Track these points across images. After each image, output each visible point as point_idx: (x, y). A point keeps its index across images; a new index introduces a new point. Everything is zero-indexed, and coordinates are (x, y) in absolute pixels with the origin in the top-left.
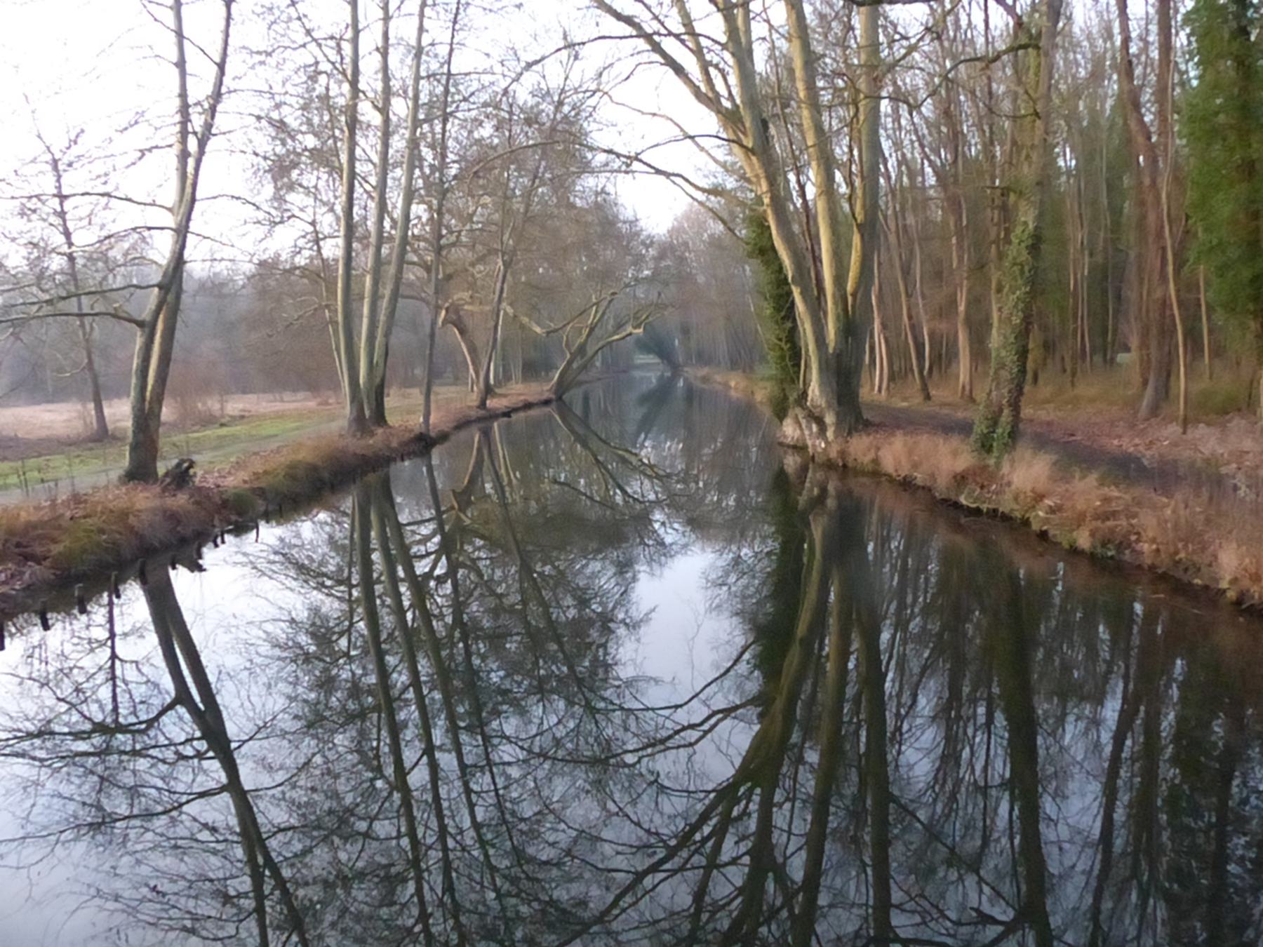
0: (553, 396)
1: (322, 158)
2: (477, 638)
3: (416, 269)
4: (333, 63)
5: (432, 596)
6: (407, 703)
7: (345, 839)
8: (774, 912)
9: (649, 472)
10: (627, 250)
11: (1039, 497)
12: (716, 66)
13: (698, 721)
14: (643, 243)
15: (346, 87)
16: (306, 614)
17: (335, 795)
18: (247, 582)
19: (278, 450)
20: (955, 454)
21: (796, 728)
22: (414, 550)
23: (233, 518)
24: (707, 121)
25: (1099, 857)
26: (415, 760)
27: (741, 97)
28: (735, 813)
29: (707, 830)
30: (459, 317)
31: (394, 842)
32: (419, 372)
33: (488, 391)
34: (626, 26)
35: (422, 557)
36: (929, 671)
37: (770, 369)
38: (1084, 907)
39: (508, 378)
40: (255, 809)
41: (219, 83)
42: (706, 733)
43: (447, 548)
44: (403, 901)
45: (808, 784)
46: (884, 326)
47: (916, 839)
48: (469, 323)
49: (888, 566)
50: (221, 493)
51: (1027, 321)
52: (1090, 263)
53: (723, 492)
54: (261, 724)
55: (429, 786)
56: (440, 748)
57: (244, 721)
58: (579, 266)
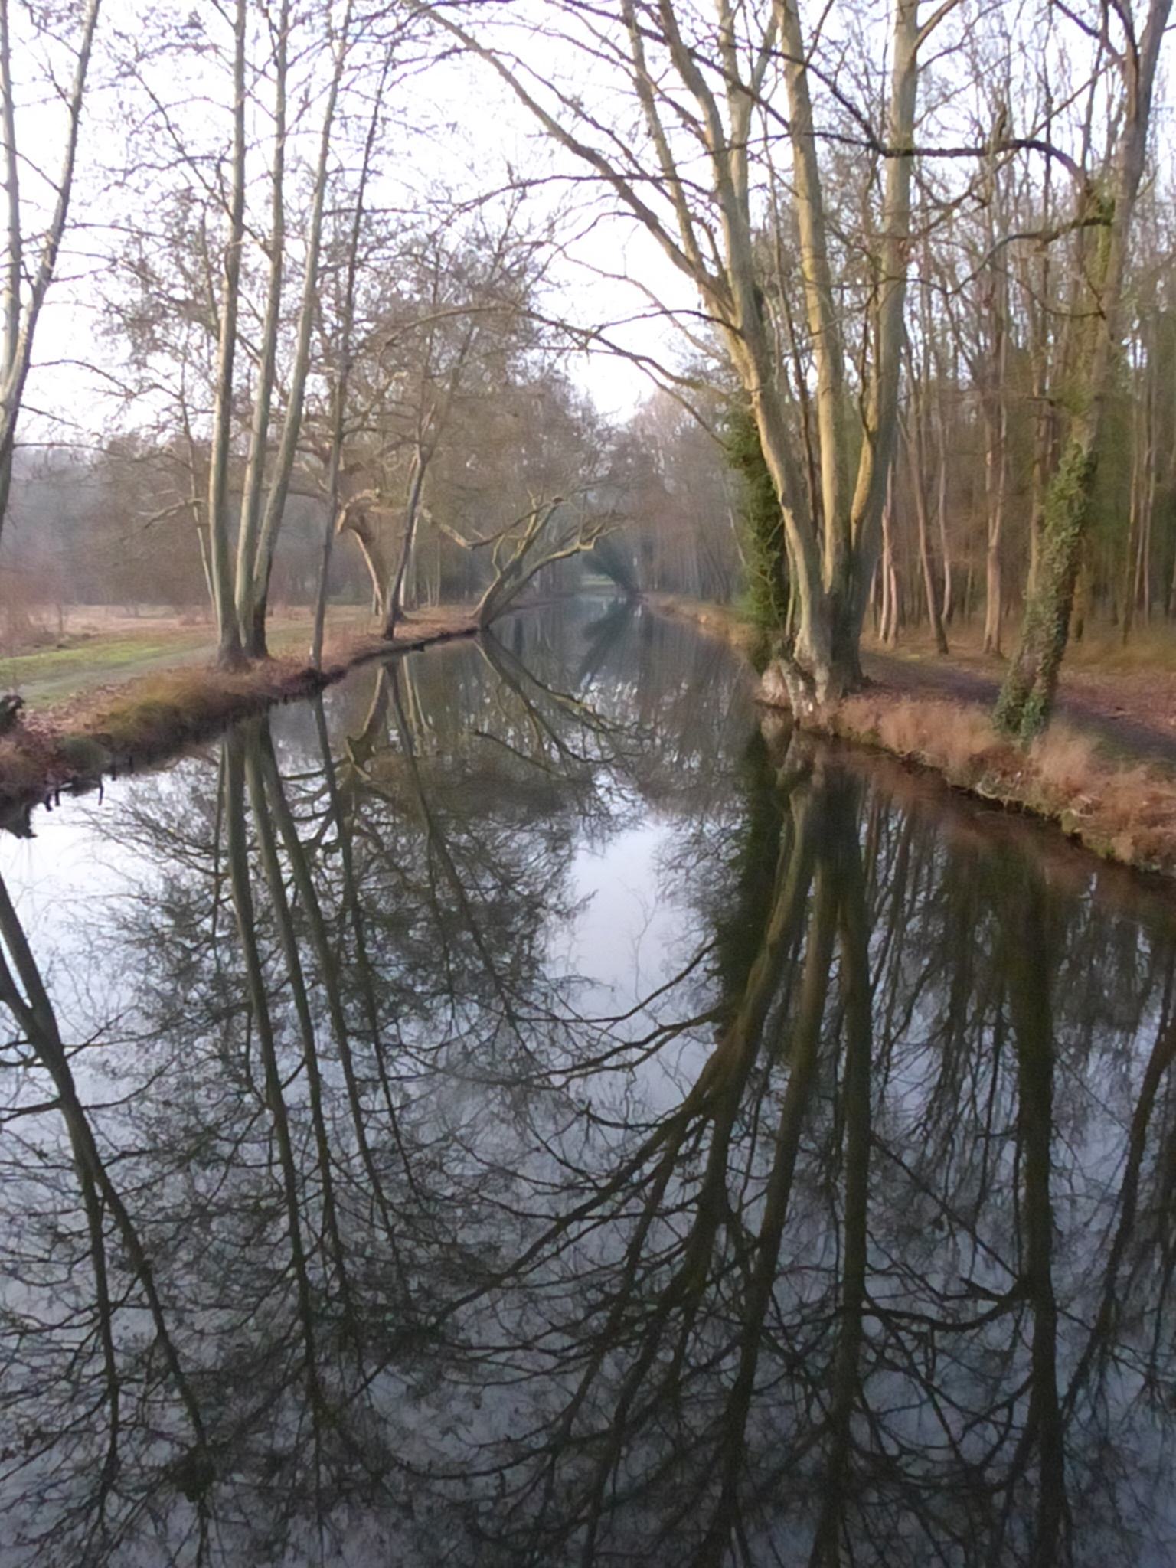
0: (478, 626)
1: (188, 310)
2: (372, 926)
3: (309, 457)
4: (211, 190)
5: (319, 868)
6: (285, 998)
7: (204, 1165)
8: (724, 1271)
9: (594, 724)
10: (578, 444)
11: (1074, 791)
12: (701, 221)
13: (641, 1039)
14: (599, 434)
15: (226, 220)
16: (161, 886)
17: (195, 1110)
18: (88, 845)
19: (130, 684)
20: (973, 730)
21: (762, 1048)
22: (299, 808)
23: (72, 773)
24: (685, 292)
25: (1119, 1215)
26: (291, 1073)
27: (731, 261)
28: (682, 1150)
29: (648, 1168)
30: (362, 519)
31: (264, 1171)
32: (310, 584)
33: (397, 616)
34: (585, 161)
35: (308, 819)
36: (926, 984)
37: (747, 604)
38: (1096, 1273)
39: (421, 598)
40: (93, 1130)
41: (62, 213)
42: (650, 1052)
43: (337, 811)
44: (273, 1239)
45: (772, 1114)
46: (896, 557)
47: (897, 1192)
48: (375, 529)
49: (884, 853)
50: (57, 740)
51: (1072, 571)
52: (1157, 490)
53: (684, 750)
54: (102, 1025)
55: (309, 1103)
56: (324, 1056)
57: (81, 1020)
58: (515, 464)
